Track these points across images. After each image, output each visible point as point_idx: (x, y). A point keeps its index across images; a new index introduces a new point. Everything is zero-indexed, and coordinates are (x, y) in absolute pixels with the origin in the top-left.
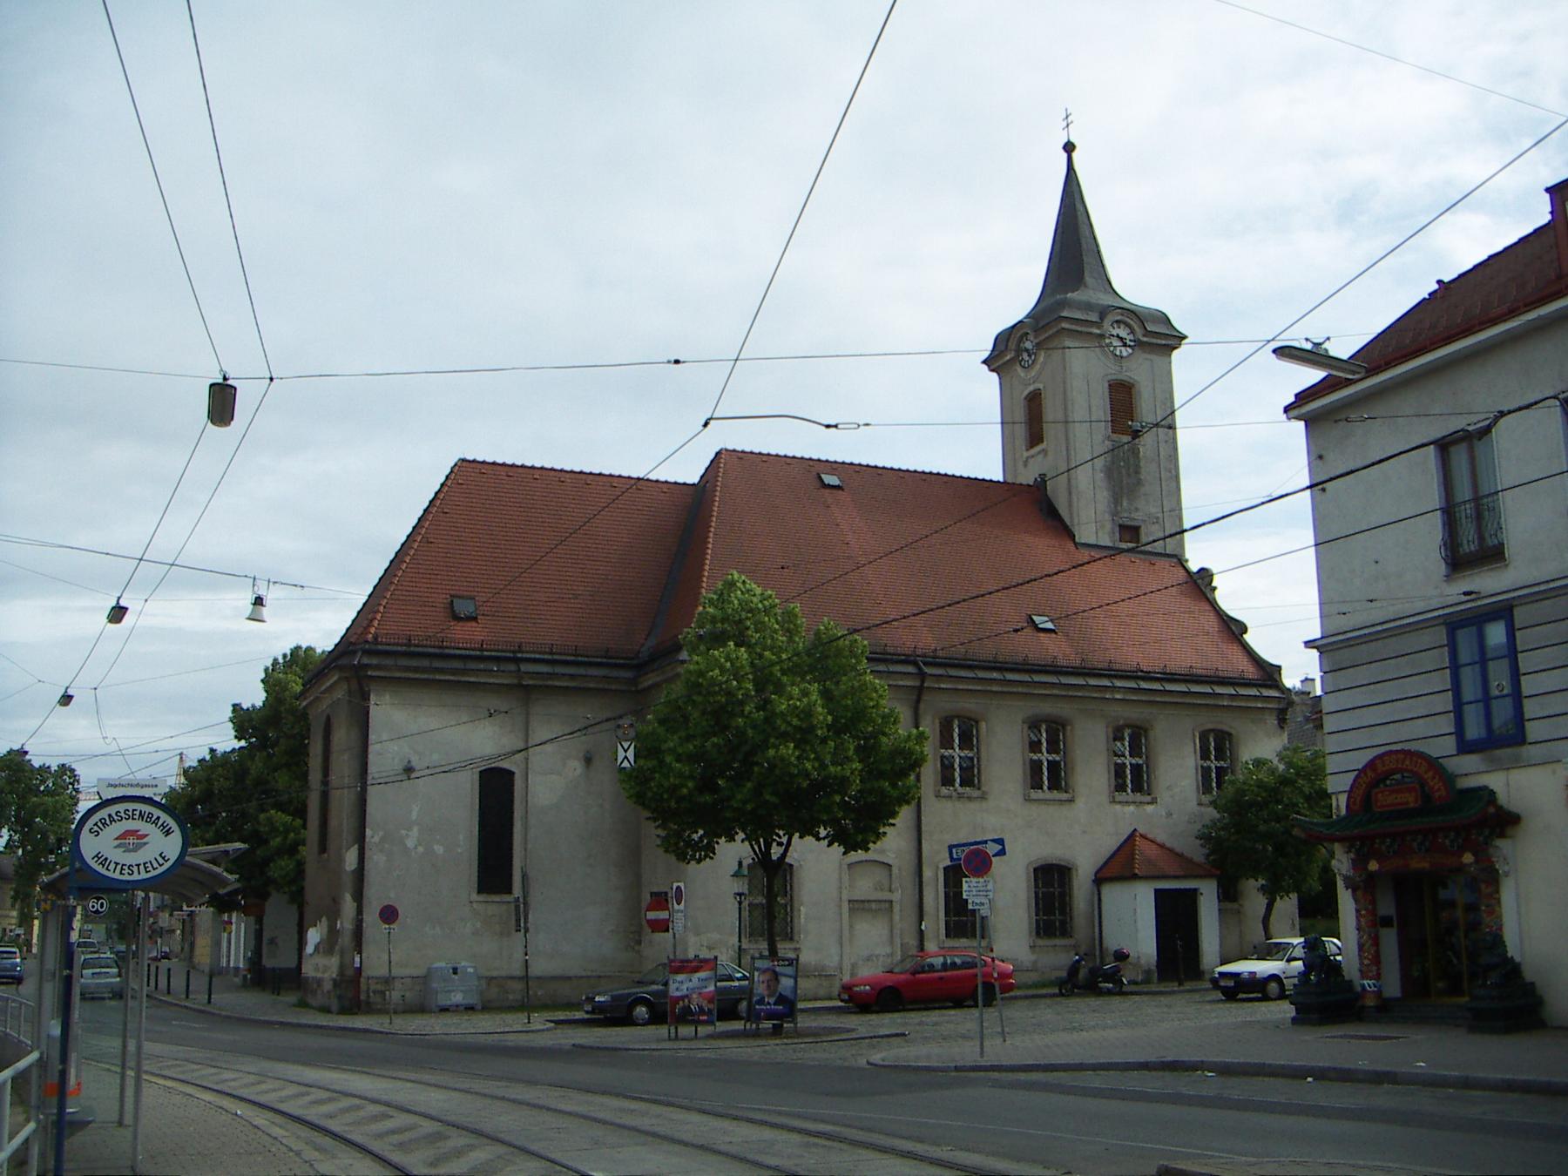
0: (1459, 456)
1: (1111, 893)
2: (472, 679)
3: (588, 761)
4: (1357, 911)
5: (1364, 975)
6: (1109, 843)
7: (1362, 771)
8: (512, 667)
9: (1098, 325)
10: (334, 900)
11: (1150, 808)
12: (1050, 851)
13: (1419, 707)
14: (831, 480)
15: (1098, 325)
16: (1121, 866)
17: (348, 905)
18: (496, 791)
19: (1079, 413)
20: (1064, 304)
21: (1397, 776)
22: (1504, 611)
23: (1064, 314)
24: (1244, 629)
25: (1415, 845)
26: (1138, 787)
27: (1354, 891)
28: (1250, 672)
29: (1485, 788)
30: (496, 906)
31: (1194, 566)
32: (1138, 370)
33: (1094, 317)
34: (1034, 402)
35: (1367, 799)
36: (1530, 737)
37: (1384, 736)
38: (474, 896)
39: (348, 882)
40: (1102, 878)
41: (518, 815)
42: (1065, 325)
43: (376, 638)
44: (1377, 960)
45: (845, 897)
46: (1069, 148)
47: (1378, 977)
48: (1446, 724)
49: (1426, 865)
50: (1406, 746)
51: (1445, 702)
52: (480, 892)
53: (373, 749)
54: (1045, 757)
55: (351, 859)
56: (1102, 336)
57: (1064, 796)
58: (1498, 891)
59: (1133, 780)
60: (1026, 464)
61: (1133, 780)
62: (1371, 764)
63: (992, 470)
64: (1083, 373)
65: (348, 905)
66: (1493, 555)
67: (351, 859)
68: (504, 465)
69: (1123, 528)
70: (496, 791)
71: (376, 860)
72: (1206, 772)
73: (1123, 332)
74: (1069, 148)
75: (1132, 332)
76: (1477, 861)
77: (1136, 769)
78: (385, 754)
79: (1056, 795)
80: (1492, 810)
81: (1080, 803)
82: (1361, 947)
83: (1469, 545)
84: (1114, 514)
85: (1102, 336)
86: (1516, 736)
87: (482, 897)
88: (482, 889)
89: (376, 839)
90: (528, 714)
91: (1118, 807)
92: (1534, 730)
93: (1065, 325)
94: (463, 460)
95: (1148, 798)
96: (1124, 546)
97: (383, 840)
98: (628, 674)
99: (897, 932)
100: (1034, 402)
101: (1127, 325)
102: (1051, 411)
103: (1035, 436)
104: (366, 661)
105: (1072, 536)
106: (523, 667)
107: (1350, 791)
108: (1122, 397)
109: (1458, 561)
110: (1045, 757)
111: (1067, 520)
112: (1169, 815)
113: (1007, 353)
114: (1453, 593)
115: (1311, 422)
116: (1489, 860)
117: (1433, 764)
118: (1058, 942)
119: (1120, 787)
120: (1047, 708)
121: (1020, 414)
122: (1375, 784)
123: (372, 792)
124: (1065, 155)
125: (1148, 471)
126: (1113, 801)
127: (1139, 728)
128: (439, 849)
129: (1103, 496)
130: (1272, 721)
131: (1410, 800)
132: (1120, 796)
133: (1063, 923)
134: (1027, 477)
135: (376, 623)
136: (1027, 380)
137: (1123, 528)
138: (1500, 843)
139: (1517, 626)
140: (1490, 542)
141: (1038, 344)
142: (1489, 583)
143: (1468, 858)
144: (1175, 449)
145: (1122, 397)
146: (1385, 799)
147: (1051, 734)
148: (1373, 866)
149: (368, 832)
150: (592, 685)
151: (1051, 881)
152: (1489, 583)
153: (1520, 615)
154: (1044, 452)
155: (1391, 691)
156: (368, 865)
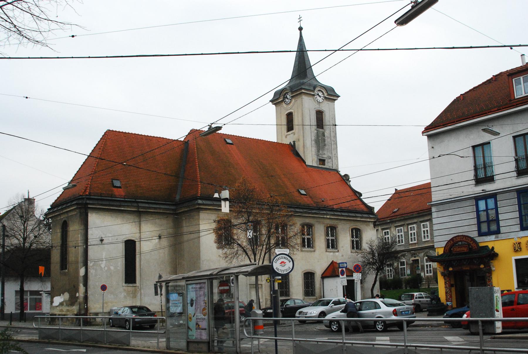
0: (479, 151)
1: (327, 281)
2: (123, 209)
3: (160, 237)
4: (445, 282)
5: (447, 301)
6: (325, 265)
7: (449, 241)
8: (135, 205)
9: (313, 91)
10: (74, 287)
11: (337, 253)
12: (308, 268)
13: (466, 223)
14: (229, 141)
15: (313, 91)
16: (332, 271)
17: (82, 288)
18: (130, 247)
19: (307, 122)
20: (303, 84)
21: (460, 243)
22: (494, 196)
23: (303, 87)
24: (361, 195)
25: (465, 263)
26: (333, 247)
27: (444, 277)
28: (365, 209)
29: (487, 246)
30: (130, 287)
31: (343, 174)
32: (325, 106)
33: (312, 89)
34: (290, 117)
35: (450, 250)
36: (502, 232)
37: (453, 231)
38: (124, 284)
39: (81, 279)
40: (324, 276)
41: (137, 257)
42: (303, 91)
43: (90, 193)
44: (451, 297)
45: (248, 283)
46: (301, 29)
47: (451, 301)
48: (475, 228)
49: (468, 268)
50: (464, 234)
51: (475, 221)
52: (126, 283)
53: (90, 232)
54: (306, 237)
55: (82, 272)
56: (314, 95)
57: (312, 250)
58: (491, 275)
59: (332, 245)
60: (286, 137)
61: (332, 245)
62: (452, 239)
63: (273, 138)
64: (306, 107)
65: (82, 288)
66: (490, 179)
67: (82, 272)
68: (122, 132)
69: (320, 160)
70: (130, 247)
71: (91, 272)
72: (353, 241)
73: (320, 94)
74: (301, 29)
75: (323, 94)
76: (485, 267)
77: (357, 241)
78: (93, 234)
79: (333, 250)
80: (493, 252)
81: (317, 252)
82: (446, 293)
83: (481, 175)
84: (318, 155)
85: (314, 95)
86: (497, 232)
87: (126, 285)
88: (126, 282)
89: (91, 265)
90: (140, 221)
91: (328, 253)
92: (502, 230)
93: (303, 91)
94: (109, 130)
95: (336, 250)
96: (320, 166)
97: (93, 265)
98: (173, 207)
99: (264, 295)
100: (290, 117)
101: (322, 92)
102: (296, 121)
103: (290, 127)
104: (88, 202)
105: (305, 163)
106: (140, 205)
107: (445, 247)
108: (320, 115)
109: (478, 181)
110: (306, 237)
111: (303, 157)
112: (342, 256)
113: (279, 98)
114: (479, 189)
115: (429, 137)
116: (490, 266)
117: (472, 239)
118: (311, 297)
119: (328, 247)
120: (308, 221)
121: (284, 121)
122: (453, 245)
123: (89, 247)
124: (299, 31)
125: (327, 141)
126: (327, 251)
127: (333, 227)
128: (112, 268)
129: (314, 149)
130: (372, 225)
131: (465, 250)
132: (328, 250)
133: (312, 291)
134: (287, 141)
135: (88, 188)
136: (286, 109)
137: (320, 160)
138: (491, 261)
139: (498, 200)
140: (489, 174)
141: (292, 97)
142: (489, 187)
143: (482, 266)
144: (336, 134)
145: (320, 115)
146: (457, 249)
147: (332, 230)
148: (451, 269)
149: (89, 263)
150: (161, 211)
151: (309, 277)
152: (489, 187)
153: (499, 197)
154: (294, 134)
155: (457, 218)
156: (89, 274)
